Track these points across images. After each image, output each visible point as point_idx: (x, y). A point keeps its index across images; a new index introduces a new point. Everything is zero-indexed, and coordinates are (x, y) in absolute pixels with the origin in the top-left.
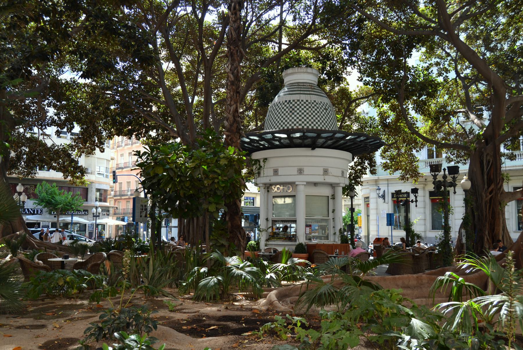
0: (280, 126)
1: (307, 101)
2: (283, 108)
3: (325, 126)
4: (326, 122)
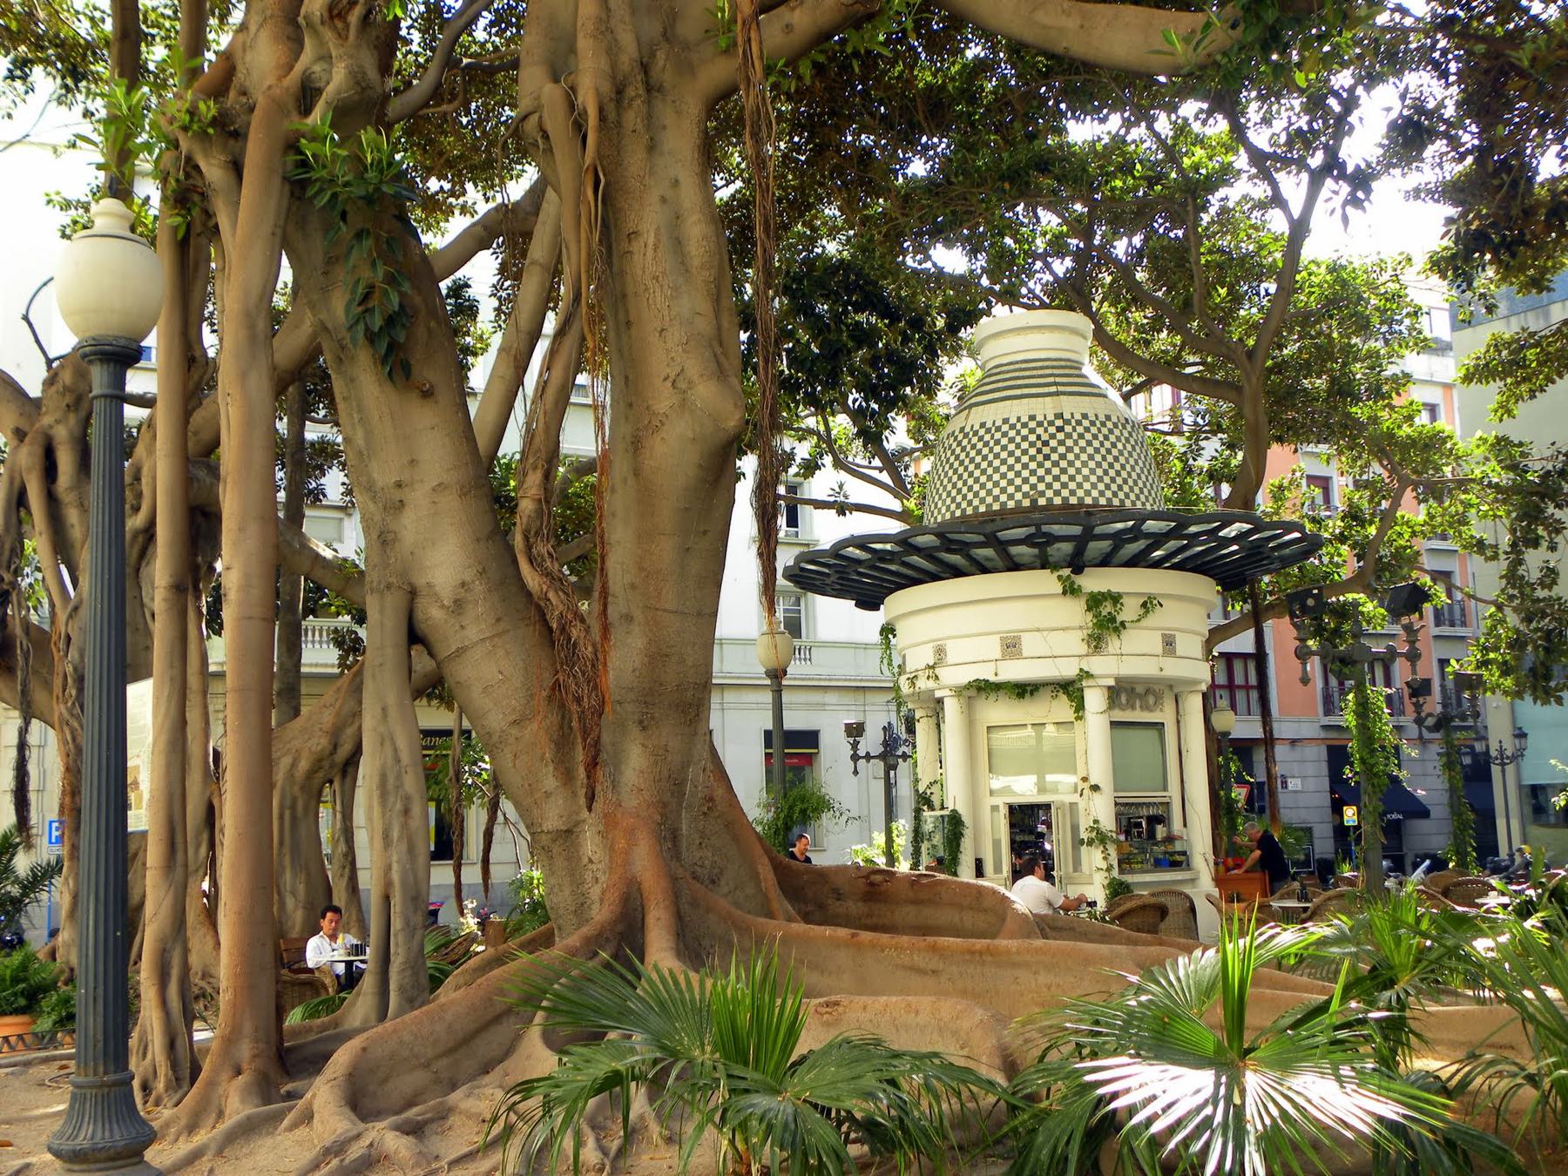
0: (964, 505)
1: (1032, 418)
2: (974, 447)
3: (1121, 495)
4: (1125, 481)
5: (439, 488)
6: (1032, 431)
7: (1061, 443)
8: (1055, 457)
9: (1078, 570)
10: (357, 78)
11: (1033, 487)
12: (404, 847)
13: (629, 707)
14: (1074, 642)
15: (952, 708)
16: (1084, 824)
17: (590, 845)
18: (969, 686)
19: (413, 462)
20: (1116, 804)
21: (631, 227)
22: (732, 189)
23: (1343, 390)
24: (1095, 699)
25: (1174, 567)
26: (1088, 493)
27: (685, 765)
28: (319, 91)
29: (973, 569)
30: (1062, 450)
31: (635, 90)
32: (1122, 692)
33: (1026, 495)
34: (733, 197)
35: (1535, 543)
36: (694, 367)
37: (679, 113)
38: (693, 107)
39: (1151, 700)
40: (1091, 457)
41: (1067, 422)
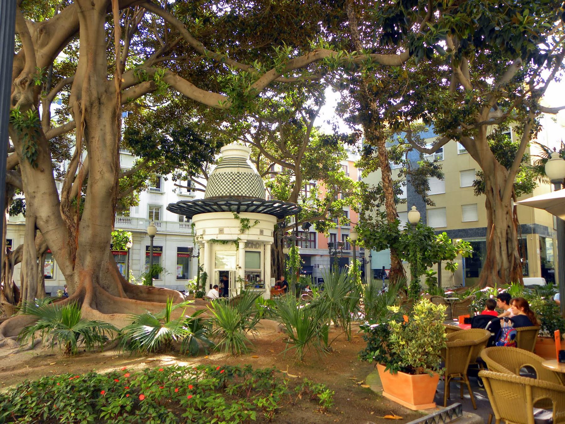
1: (232, 173)
5: (44, 193)
6: (231, 176)
7: (238, 180)
8: (236, 183)
9: (238, 213)
10: (27, 99)
11: (230, 190)
12: (31, 277)
13: (87, 247)
14: (237, 231)
15: (206, 245)
16: (237, 276)
17: (76, 279)
18: (210, 240)
19: (38, 187)
20: (245, 272)
21: (93, 136)
22: (168, 103)
23: (326, 168)
24: (242, 245)
25: (265, 213)
26: (244, 193)
27: (101, 261)
28: (17, 101)
29: (212, 210)
30: (238, 181)
31: (96, 104)
32: (248, 243)
33: (228, 192)
34: (168, 105)
35: (367, 209)
36: (105, 169)
37: (107, 109)
38: (110, 109)
39: (257, 246)
40: (246, 184)
41: (240, 174)
